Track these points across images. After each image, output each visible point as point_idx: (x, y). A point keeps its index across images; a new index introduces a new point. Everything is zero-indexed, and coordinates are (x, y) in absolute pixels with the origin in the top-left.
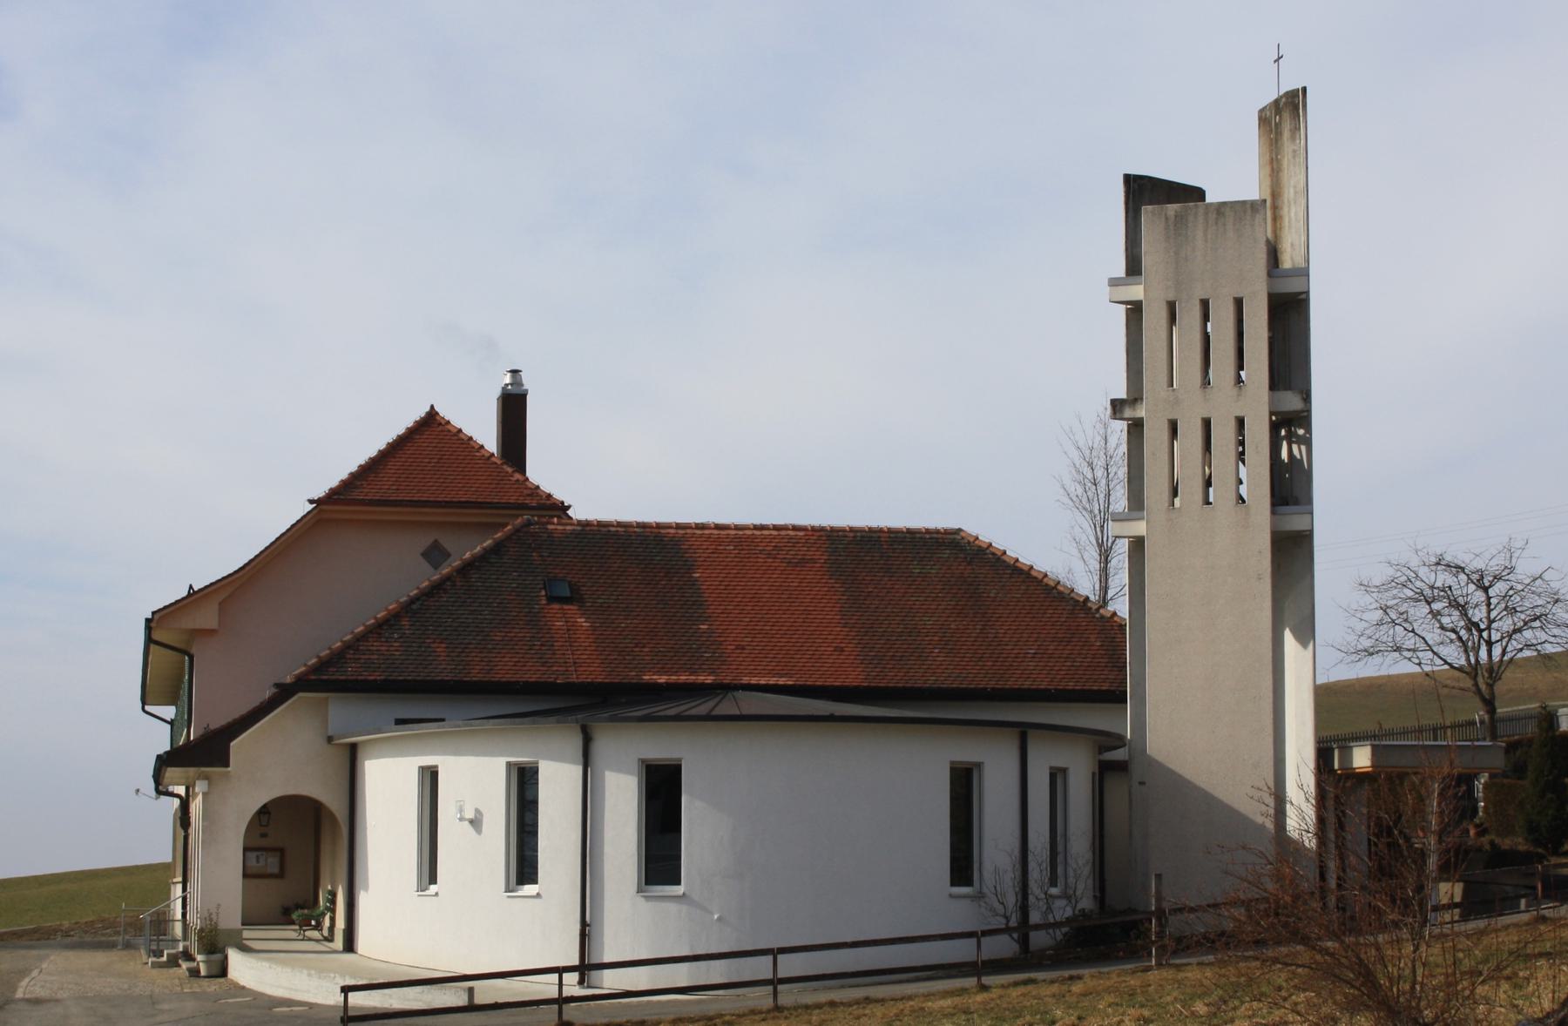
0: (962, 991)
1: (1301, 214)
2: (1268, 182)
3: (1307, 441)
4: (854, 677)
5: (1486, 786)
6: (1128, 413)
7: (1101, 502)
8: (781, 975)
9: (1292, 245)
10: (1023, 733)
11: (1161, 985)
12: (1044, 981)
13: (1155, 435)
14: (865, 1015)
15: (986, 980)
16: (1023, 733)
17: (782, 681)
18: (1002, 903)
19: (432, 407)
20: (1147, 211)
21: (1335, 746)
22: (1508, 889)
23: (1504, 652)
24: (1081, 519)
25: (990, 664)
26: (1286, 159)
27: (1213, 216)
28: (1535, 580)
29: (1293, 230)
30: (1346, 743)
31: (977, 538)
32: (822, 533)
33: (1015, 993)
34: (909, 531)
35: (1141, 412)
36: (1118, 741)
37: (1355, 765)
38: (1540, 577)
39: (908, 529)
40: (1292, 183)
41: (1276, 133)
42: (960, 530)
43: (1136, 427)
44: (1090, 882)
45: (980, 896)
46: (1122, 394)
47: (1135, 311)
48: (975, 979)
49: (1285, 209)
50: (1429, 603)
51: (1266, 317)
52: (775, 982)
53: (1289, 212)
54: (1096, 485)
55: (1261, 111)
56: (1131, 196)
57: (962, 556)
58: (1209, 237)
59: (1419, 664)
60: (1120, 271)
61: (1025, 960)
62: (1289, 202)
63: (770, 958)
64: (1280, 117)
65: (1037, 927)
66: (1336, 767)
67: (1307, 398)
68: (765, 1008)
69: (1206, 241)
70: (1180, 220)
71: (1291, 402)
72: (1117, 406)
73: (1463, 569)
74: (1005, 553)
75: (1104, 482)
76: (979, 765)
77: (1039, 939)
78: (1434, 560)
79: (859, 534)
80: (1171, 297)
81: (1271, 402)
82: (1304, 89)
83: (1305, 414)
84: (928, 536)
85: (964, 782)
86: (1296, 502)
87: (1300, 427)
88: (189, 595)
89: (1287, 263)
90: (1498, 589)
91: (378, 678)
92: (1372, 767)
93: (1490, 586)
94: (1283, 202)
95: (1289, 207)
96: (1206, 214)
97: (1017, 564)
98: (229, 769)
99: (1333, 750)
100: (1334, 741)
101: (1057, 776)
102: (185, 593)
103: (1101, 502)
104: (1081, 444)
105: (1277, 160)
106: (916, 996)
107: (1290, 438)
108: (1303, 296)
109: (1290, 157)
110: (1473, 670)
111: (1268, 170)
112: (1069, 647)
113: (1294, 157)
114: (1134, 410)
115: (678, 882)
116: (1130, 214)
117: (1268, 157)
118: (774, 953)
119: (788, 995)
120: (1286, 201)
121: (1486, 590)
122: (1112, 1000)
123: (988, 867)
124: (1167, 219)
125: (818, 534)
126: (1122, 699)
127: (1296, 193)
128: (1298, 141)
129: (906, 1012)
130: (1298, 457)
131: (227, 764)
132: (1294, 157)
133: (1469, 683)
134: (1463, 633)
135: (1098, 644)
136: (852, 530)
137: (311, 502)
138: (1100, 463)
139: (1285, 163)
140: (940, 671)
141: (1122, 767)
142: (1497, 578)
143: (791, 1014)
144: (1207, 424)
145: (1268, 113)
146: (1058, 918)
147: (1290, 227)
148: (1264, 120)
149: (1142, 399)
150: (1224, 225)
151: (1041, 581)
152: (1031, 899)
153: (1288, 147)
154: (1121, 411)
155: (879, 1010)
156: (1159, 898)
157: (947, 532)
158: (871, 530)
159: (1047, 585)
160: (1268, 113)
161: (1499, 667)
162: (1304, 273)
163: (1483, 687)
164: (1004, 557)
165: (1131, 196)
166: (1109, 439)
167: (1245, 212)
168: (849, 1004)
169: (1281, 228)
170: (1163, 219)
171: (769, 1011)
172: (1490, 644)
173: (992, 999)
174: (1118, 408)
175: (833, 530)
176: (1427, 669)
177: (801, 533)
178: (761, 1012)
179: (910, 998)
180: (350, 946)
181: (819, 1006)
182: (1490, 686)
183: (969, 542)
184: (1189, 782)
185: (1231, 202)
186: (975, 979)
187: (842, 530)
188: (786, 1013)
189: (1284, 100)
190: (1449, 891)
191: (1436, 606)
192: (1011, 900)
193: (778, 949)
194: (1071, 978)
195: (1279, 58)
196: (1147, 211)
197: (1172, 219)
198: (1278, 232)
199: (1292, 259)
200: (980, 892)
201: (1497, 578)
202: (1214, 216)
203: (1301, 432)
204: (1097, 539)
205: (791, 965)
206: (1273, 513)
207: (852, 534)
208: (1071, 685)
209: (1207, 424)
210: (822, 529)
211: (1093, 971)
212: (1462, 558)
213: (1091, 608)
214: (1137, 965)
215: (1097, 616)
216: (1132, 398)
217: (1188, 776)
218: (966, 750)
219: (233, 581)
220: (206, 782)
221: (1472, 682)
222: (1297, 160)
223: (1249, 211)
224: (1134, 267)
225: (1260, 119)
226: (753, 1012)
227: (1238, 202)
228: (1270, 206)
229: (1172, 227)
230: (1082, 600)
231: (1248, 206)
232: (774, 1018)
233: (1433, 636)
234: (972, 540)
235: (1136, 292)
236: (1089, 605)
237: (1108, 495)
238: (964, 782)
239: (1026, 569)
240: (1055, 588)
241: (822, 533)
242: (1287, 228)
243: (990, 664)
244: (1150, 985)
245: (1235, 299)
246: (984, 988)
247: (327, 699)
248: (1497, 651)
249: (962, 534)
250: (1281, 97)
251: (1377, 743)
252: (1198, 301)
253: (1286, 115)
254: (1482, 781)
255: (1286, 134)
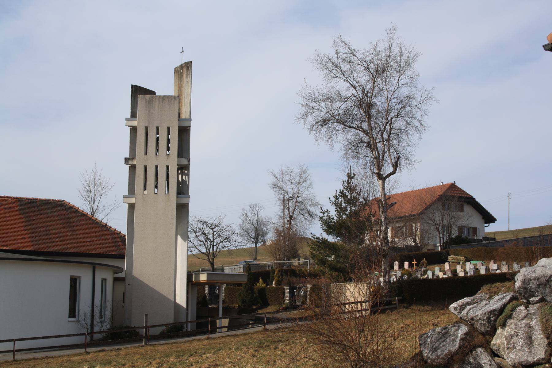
0: (80, 354)
1: (189, 102)
2: (177, 91)
3: (188, 175)
4: (29, 248)
5: (225, 289)
6: (130, 162)
7: (92, 198)
8: (16, 348)
9: (185, 111)
10: (94, 267)
11: (151, 352)
12: (108, 350)
13: (139, 171)
14: (50, 363)
15: (89, 350)
16: (94, 267)
17: (4, 248)
18: (86, 324)
20: (140, 97)
21: (193, 273)
22: (245, 320)
23: (217, 248)
24: (86, 203)
25: (75, 244)
26: (184, 84)
27: (161, 100)
28: (227, 227)
29: (186, 107)
30: (197, 273)
31: (69, 203)
32: (17, 199)
33: (102, 354)
34: (47, 200)
35: (135, 162)
36: (121, 270)
37: (200, 280)
38: (230, 226)
39: (46, 199)
40: (186, 92)
41: (181, 75)
42: (64, 200)
43: (133, 168)
44: (90, 314)
45: (78, 321)
46: (128, 156)
47: (134, 130)
48: (84, 349)
49: (183, 100)
50: (195, 233)
51: (177, 134)
52: (14, 351)
53: (185, 101)
54: (91, 192)
55: (175, 68)
56: (133, 92)
57: (64, 209)
58: (160, 106)
59: (191, 252)
60: (129, 116)
61: (92, 344)
62: (185, 97)
63: (13, 342)
64: (183, 71)
65: (97, 333)
66: (194, 280)
67: (189, 161)
68: (10, 360)
69: (159, 108)
70: (151, 101)
71: (184, 162)
72: (127, 160)
73: (206, 222)
74: (79, 208)
75: (93, 191)
76: (79, 277)
77: (97, 337)
78: (197, 219)
79: (29, 200)
80: (146, 126)
81: (178, 161)
82: (191, 62)
83: (188, 166)
84: (53, 202)
85: (74, 282)
86: (184, 194)
87: (186, 170)
89: (183, 117)
90: (216, 229)
92: (207, 280)
93: (214, 228)
94: (183, 97)
95: (185, 99)
96: (159, 99)
97: (83, 212)
99: (192, 275)
100: (193, 272)
101: (104, 281)
103: (92, 198)
104: (87, 179)
105: (181, 84)
106: (64, 356)
107: (182, 174)
108: (188, 128)
109: (186, 82)
110: (208, 254)
111: (177, 87)
112: (101, 240)
113: (187, 83)
114: (132, 161)
116: (133, 98)
117: (177, 83)
118: (14, 341)
119: (18, 356)
120: (184, 97)
121: (213, 229)
122: (139, 357)
123: (81, 312)
124: (146, 100)
125: (16, 199)
126: (123, 257)
127: (187, 95)
128: (188, 78)
129: (64, 361)
130: (185, 180)
132: (187, 83)
133: (206, 258)
134: (204, 242)
135: (110, 239)
136: (27, 199)
138: (92, 185)
139: (184, 85)
140: (58, 246)
141: (122, 280)
142: (216, 226)
143: (21, 363)
144: (157, 167)
145: (178, 69)
146: (105, 329)
147: (185, 105)
148: (176, 71)
149: (135, 158)
150: (165, 103)
151: (91, 218)
152: (95, 322)
153: (185, 79)
154: (128, 162)
155: (54, 361)
156: (146, 322)
157: (59, 201)
158: (34, 199)
159: (93, 219)
160: (178, 69)
161: (216, 253)
162: (190, 120)
163: (211, 259)
164: (79, 210)
165: (133, 92)
166: (96, 178)
167: (172, 99)
168: (41, 359)
169: (181, 106)
170: (145, 99)
171: (12, 361)
172: (213, 246)
173: (94, 357)
174: (127, 161)
175: (21, 198)
176: (194, 253)
177: (10, 199)
178: (9, 362)
179: (63, 356)
181: (30, 360)
182: (213, 259)
183: (67, 205)
184: (146, 284)
185: (167, 96)
186: (84, 349)
187: (24, 199)
188: (18, 362)
189: (184, 65)
190: (225, 322)
191: (197, 234)
192: (89, 323)
193: (16, 339)
194: (118, 349)
195: (182, 52)
196: (140, 97)
197: (148, 100)
198: (180, 107)
199: (185, 116)
200: (78, 320)
201: (216, 226)
202: (162, 100)
203: (186, 172)
204: (91, 210)
205: (20, 345)
206: (177, 197)
207: (27, 200)
208: (102, 252)
209: (157, 167)
210: (17, 198)
211: (125, 346)
212: (207, 220)
213: (107, 228)
214: (139, 344)
215: (110, 230)
216: (132, 158)
217: (146, 282)
218: (75, 271)
221: (208, 257)
222: (188, 84)
223: (173, 99)
224: (134, 115)
225: (175, 71)
226: (6, 362)
227: (170, 96)
228: (178, 98)
229: (148, 102)
230: (105, 225)
231: (173, 98)
232: (15, 364)
233: (196, 242)
234: (68, 204)
235: (135, 123)
236: (107, 226)
237: (95, 195)
238: (74, 282)
239: (86, 214)
240: (95, 221)
241: (17, 199)
242: (184, 106)
243: (75, 244)
244: (147, 352)
246: (88, 353)
248: (215, 248)
249: (64, 202)
250: (183, 64)
251: (208, 273)
252: (155, 127)
253: (185, 70)
254: (224, 287)
255: (185, 76)
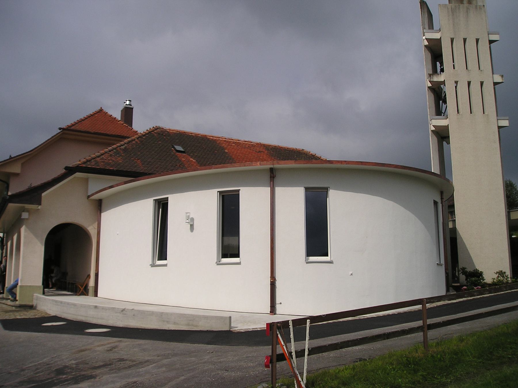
19: (101, 108)
88: (10, 159)
91: (115, 169)
98: (40, 207)
102: (8, 158)
115: (326, 255)
124: (448, 9)
131: (40, 204)
137: (60, 129)
165: (422, 6)
180: (96, 295)
219: (29, 155)
220: (28, 213)
229: (450, 12)
245: (476, 39)
247: (87, 180)
